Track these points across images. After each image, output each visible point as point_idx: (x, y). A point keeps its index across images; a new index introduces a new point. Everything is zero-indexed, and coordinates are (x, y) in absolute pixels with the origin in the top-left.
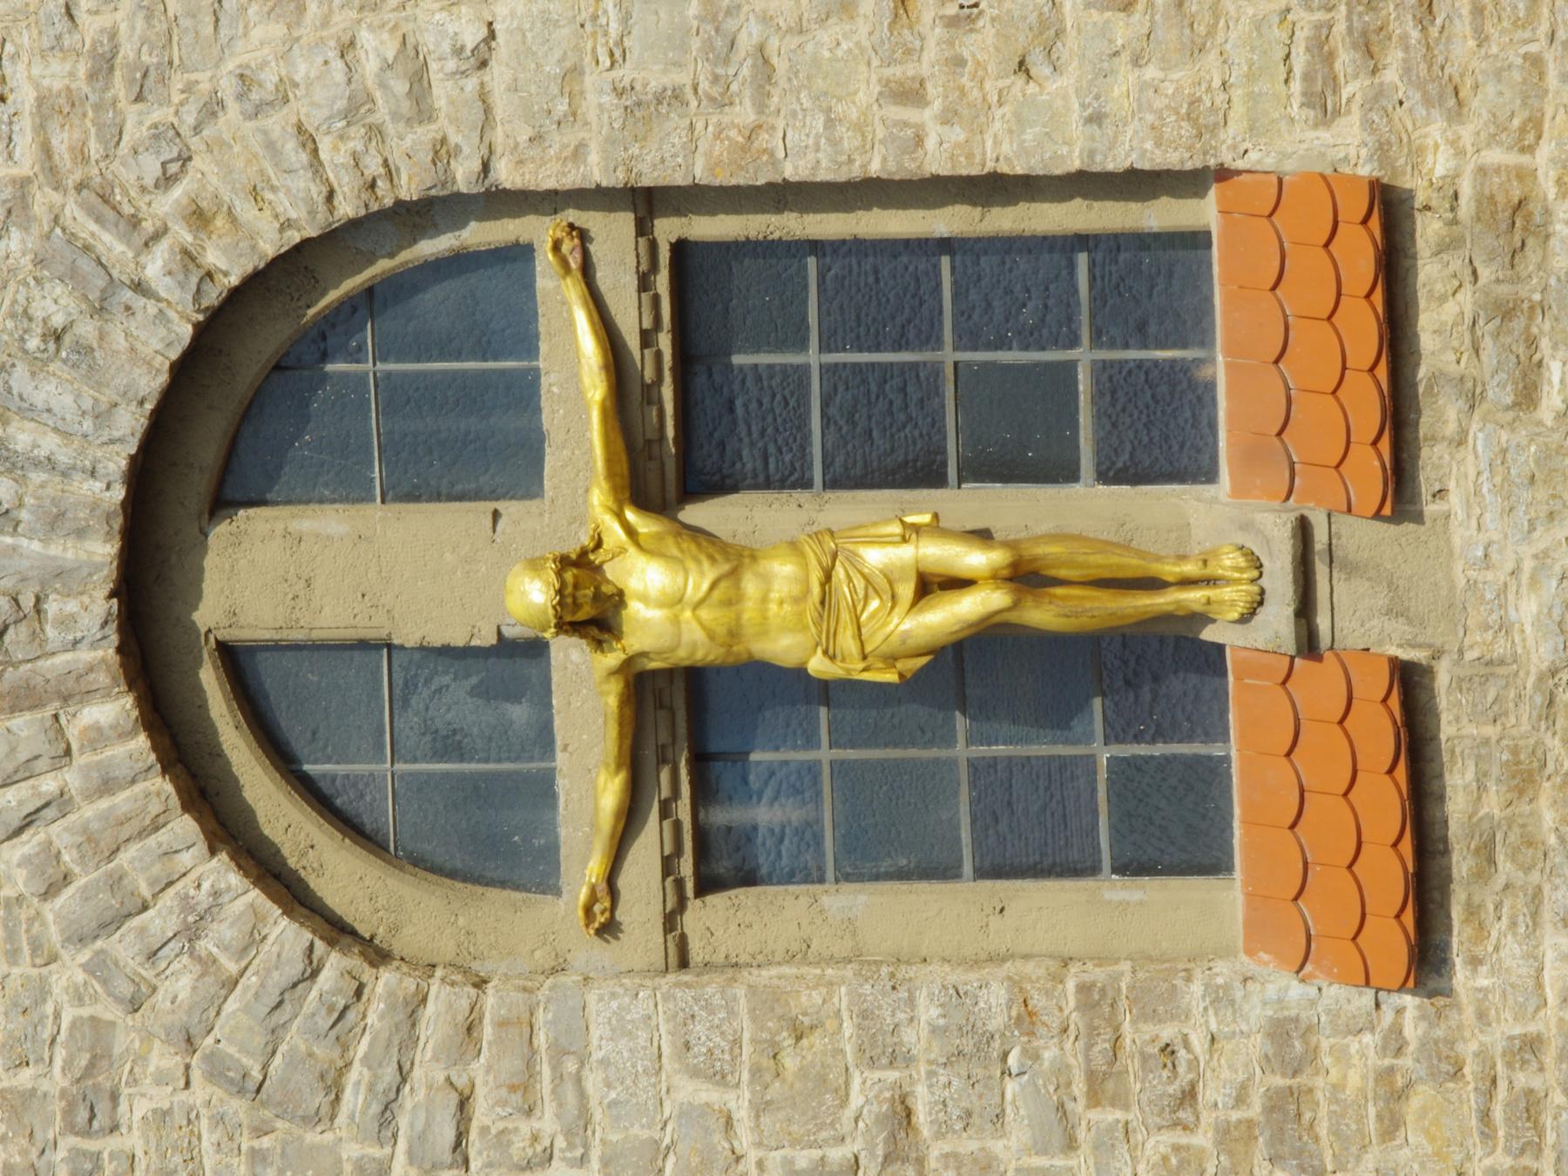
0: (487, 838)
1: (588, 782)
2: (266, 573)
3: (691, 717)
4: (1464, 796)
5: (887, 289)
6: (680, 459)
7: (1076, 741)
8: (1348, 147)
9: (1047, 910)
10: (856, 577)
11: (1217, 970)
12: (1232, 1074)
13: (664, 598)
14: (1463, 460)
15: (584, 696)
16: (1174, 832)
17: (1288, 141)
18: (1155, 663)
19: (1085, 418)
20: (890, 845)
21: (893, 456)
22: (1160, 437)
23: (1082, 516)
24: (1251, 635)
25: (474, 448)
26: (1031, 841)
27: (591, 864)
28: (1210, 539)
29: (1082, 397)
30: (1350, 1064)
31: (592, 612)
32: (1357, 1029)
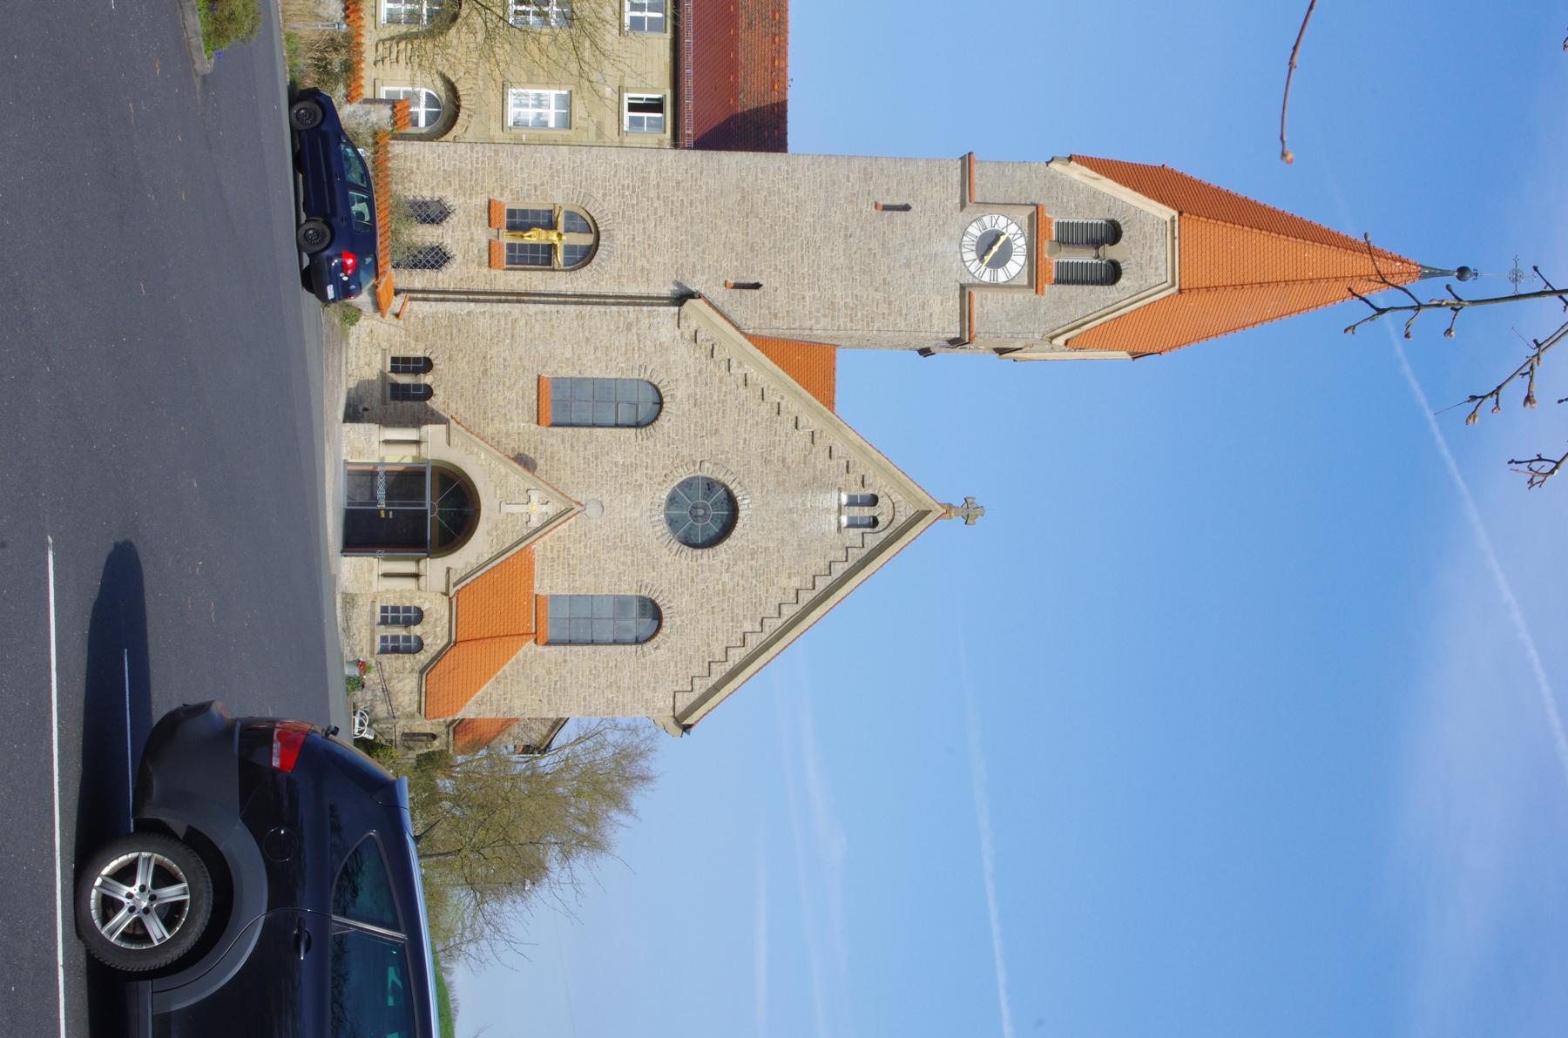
0: (571, 216)
1: (561, 220)
2: (587, 240)
3: (551, 225)
4: (486, 216)
5: (534, 261)
6: (551, 248)
7: (519, 221)
8: (493, 272)
9: (523, 207)
10: (535, 237)
11: (508, 201)
12: (507, 193)
13: (553, 237)
14: (485, 244)
15: (561, 228)
16: (511, 213)
17: (499, 272)
18: (512, 227)
19: (60, 961)
20: (536, 213)
21: (534, 247)
22: (511, 247)
23: (517, 241)
24: (504, 231)
25: (569, 249)
26: (524, 213)
27: (534, 240)
28: (507, 238)
29: (691, 59)
30: (497, 193)
31: (559, 235)
32: (496, 196)
